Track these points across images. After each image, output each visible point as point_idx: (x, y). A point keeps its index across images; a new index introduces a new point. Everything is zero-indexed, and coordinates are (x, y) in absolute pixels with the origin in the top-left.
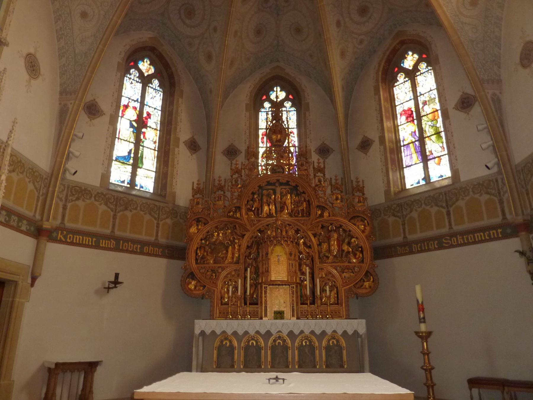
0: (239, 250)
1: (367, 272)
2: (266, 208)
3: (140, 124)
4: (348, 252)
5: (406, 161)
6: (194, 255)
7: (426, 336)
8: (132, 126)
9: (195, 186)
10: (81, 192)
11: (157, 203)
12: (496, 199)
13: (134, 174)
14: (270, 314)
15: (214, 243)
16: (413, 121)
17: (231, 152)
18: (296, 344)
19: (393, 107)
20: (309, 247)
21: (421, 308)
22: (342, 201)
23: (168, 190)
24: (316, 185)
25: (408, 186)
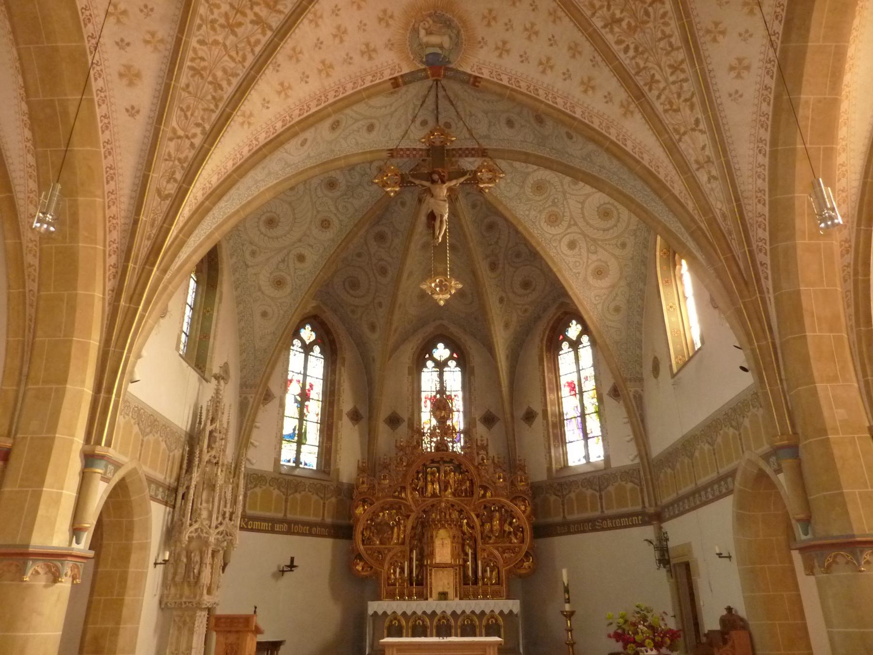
0: (405, 531)
1: (527, 552)
2: (430, 487)
3: (304, 396)
4: (510, 533)
5: (569, 436)
6: (360, 536)
7: (570, 615)
8: (296, 401)
9: (360, 464)
10: (256, 479)
11: (324, 483)
12: (638, 488)
13: (298, 452)
14: (435, 594)
15: (379, 524)
16: (575, 395)
17: (394, 421)
18: (459, 623)
19: (557, 376)
20: (473, 528)
21: (567, 590)
22: (504, 480)
23: (332, 467)
24: (480, 464)
25: (571, 464)
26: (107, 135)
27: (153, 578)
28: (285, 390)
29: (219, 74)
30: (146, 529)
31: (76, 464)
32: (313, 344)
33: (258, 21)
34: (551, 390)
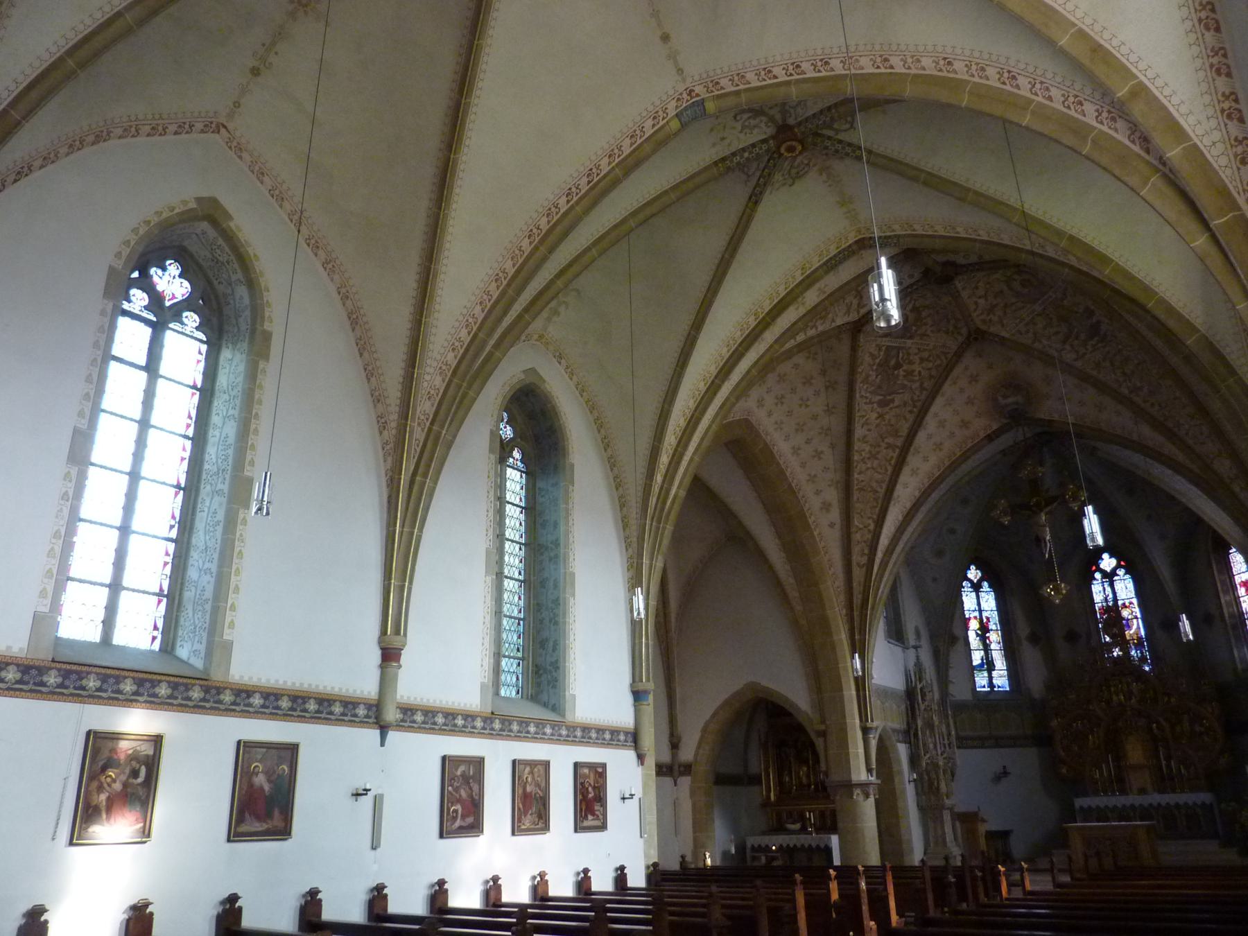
2: (1115, 698)
3: (984, 629)
8: (978, 635)
10: (960, 707)
13: (991, 678)
17: (1072, 637)
19: (1231, 577)
26: (823, 544)
27: (910, 790)
28: (967, 629)
29: (874, 484)
30: (899, 761)
31: (859, 734)
32: (980, 581)
33: (889, 446)
34: (1226, 592)
